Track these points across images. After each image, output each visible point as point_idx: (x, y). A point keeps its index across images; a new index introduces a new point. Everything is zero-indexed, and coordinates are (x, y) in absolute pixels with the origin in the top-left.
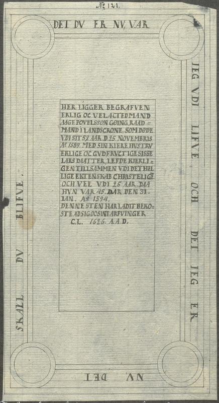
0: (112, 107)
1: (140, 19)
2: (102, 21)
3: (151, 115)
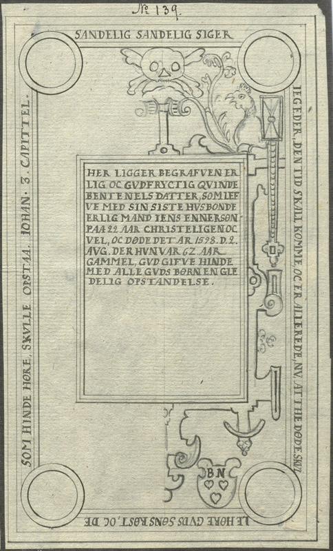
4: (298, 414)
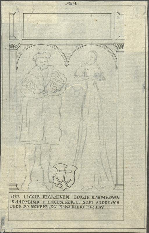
0: (46, 197)
1: (35, 195)
2: (18, 196)
3: (39, 201)
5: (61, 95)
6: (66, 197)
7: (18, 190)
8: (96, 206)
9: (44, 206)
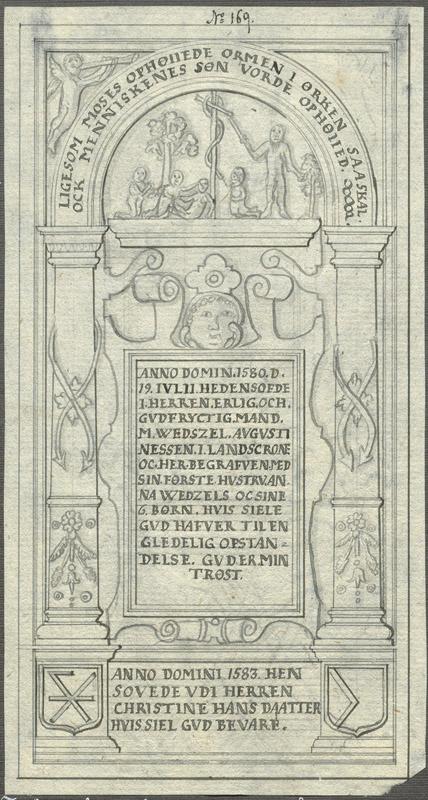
4: (233, 692)
5: (364, 567)
6: (182, 448)
7: (118, 750)
8: (216, 499)
9: (262, 557)
